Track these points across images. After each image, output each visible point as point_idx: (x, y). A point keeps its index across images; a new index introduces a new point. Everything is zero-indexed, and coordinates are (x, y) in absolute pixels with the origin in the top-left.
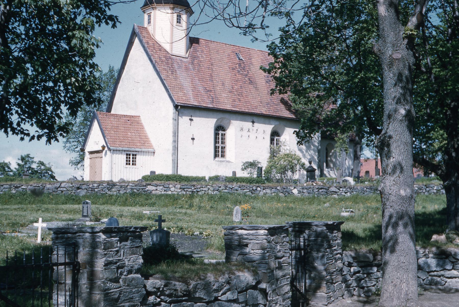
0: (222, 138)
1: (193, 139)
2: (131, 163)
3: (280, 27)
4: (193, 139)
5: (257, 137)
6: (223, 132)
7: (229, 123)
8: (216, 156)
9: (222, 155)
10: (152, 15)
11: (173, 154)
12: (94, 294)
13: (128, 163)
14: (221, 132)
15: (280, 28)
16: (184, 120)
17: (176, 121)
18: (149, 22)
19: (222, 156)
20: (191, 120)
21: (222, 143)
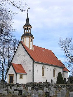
8: (42, 76)
16: (35, 65)
17: (33, 66)
20: (37, 66)
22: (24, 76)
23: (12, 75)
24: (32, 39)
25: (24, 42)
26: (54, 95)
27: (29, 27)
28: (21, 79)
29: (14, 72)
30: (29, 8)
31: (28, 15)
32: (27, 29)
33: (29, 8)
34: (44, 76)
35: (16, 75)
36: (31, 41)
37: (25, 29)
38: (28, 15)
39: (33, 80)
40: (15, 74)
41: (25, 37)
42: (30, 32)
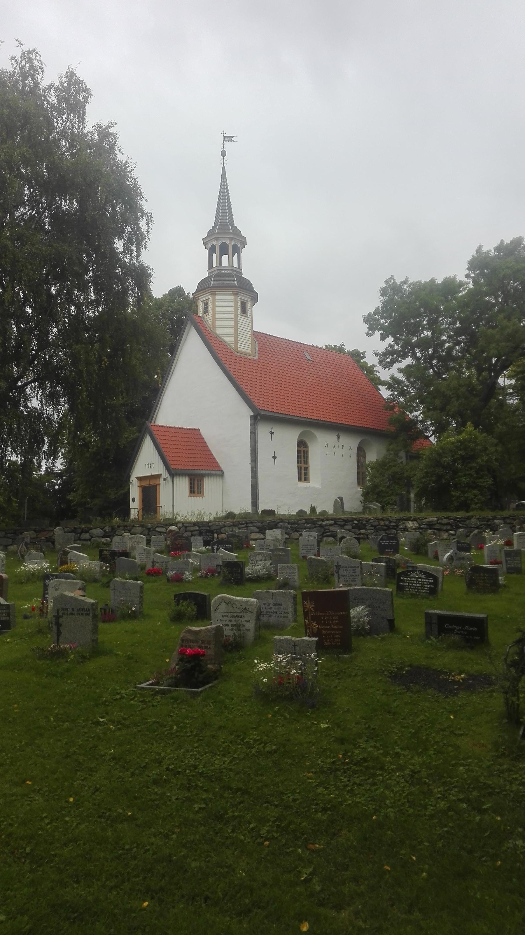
0: (304, 457)
1: (274, 458)
2: (196, 490)
3: (436, 278)
4: (274, 458)
5: (343, 455)
6: (305, 449)
7: (314, 437)
8: (300, 479)
9: (305, 478)
10: (210, 302)
11: (252, 477)
12: (235, 639)
13: (192, 491)
14: (302, 449)
15: (368, 319)
16: (263, 430)
17: (254, 434)
18: (206, 311)
19: (305, 480)
20: (272, 433)
21: (304, 463)
22: (209, 484)
23: (153, 482)
24: (249, 305)
25: (209, 318)
26: (403, 778)
27: (231, 239)
28: (303, 484)
29: (159, 469)
30: (228, 139)
31: (224, 175)
32: (224, 250)
33: (228, 139)
34: (306, 479)
35: (169, 479)
36: (244, 311)
37: (212, 250)
38: (224, 175)
39: (255, 503)
40: (165, 474)
41: (213, 294)
42: (236, 265)
